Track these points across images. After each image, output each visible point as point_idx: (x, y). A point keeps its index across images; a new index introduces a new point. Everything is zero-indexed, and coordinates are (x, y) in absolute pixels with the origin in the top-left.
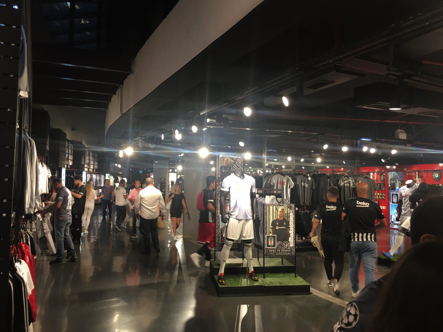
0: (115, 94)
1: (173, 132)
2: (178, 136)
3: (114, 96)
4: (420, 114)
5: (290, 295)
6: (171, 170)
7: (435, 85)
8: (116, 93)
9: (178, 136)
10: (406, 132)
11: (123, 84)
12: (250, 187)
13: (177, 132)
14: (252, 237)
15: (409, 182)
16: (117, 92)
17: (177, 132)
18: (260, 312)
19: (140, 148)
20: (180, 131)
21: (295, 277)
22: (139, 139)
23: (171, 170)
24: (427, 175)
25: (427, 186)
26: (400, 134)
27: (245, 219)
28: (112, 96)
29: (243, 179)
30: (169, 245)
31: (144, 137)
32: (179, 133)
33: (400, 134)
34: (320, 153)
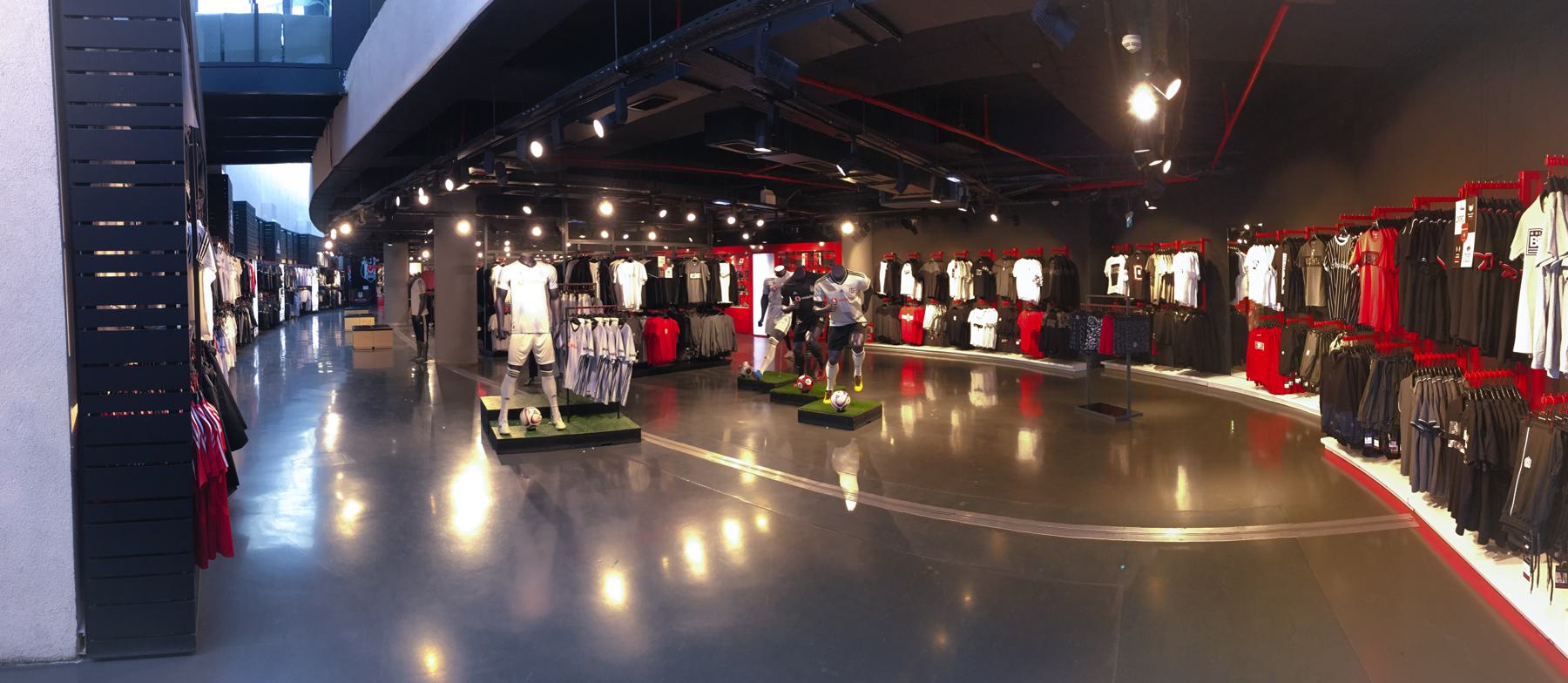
2: (423, 199)
9: (423, 199)
13: (421, 191)
20: (427, 192)
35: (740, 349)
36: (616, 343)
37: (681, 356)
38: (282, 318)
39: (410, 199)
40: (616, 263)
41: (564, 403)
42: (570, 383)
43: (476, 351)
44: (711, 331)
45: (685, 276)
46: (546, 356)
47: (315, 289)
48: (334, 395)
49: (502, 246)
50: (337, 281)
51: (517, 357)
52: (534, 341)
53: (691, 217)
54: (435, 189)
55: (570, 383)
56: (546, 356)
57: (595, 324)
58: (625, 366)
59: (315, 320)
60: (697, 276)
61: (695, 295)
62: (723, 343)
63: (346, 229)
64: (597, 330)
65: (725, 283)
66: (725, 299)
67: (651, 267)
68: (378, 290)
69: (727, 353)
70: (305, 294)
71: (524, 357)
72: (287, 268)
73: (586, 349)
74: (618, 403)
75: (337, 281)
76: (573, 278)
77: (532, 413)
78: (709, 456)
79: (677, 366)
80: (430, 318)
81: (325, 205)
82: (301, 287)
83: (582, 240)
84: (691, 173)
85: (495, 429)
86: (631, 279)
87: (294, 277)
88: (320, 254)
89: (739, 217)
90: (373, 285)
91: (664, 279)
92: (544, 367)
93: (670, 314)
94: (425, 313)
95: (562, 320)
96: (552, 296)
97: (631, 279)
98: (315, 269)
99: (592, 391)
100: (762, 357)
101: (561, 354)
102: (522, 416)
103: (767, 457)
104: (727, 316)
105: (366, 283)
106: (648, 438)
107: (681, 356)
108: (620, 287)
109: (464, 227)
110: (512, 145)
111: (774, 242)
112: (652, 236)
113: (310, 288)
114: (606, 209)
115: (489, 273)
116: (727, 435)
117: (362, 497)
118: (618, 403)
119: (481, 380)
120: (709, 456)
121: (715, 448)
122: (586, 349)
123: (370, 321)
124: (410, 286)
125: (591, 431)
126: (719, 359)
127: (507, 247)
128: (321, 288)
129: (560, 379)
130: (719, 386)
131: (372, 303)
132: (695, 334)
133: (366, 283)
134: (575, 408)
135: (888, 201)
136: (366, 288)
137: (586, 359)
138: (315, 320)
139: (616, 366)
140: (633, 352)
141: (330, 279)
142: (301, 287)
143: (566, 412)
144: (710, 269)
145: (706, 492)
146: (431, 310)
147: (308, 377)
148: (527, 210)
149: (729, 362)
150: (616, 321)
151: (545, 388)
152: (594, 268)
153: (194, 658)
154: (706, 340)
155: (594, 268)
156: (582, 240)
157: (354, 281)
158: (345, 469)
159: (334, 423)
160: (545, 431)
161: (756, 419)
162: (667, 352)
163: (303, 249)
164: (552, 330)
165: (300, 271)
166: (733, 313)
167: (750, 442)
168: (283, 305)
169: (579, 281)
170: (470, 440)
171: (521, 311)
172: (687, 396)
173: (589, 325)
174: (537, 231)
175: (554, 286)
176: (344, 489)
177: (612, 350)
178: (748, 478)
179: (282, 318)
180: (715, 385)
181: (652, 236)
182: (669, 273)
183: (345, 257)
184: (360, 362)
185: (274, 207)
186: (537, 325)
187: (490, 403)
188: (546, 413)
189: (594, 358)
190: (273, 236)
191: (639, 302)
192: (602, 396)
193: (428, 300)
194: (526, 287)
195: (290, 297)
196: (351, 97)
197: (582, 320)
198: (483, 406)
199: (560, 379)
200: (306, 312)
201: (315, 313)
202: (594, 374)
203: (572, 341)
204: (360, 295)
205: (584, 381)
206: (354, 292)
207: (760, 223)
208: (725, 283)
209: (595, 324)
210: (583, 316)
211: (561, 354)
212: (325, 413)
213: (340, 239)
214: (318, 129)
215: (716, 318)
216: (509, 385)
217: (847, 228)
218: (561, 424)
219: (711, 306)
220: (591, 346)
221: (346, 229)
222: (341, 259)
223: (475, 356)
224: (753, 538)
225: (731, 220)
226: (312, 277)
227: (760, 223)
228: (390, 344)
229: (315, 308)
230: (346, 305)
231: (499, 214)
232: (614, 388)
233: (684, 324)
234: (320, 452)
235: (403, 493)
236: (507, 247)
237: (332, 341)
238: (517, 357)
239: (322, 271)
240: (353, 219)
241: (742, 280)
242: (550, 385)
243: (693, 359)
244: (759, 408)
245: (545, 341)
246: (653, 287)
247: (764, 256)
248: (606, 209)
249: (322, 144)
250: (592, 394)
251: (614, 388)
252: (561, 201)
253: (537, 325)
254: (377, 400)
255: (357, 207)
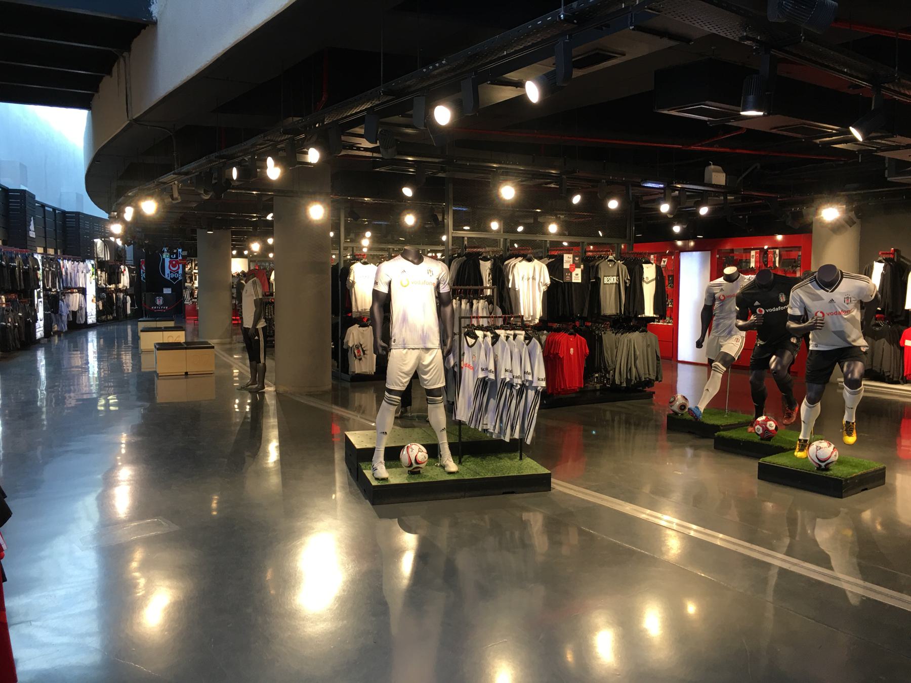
0: (109, 73)
1: (259, 163)
2: (273, 171)
3: (106, 80)
4: (774, 131)
5: (513, 493)
6: (234, 252)
7: (827, 67)
9: (273, 171)
10: (725, 171)
11: (129, 50)
12: (435, 282)
13: (270, 161)
15: (729, 270)
16: (115, 69)
17: (270, 161)
18: (896, 403)
19: (177, 199)
20: (278, 161)
21: (521, 459)
23: (234, 252)
26: (714, 174)
27: (421, 346)
28: (100, 79)
29: (418, 263)
30: (248, 407)
31: (186, 174)
32: (276, 165)
33: (714, 174)
34: (556, 215)
35: (665, 380)
36: (520, 362)
37: (598, 386)
38: (40, 332)
39: (252, 173)
40: (512, 261)
41: (455, 440)
42: (463, 413)
44: (627, 351)
45: (598, 280)
46: (435, 379)
47: (91, 292)
48: (124, 438)
49: (360, 235)
50: (125, 281)
51: (397, 379)
52: (419, 359)
53: (613, 204)
54: (290, 157)
55: (463, 413)
56: (435, 379)
57: (496, 338)
58: (531, 394)
59: (92, 337)
60: (613, 280)
61: (610, 305)
62: (643, 369)
63: (150, 207)
64: (499, 344)
65: (649, 291)
66: (649, 311)
67: (555, 268)
68: (186, 294)
69: (649, 383)
70: (75, 300)
71: (406, 380)
72: (47, 259)
73: (485, 369)
74: (522, 440)
75: (125, 281)
76: (465, 282)
77: (416, 451)
78: (628, 508)
79: (581, 397)
80: (269, 333)
81: (114, 169)
82: (69, 289)
84: (625, 152)
85: (368, 473)
86: (529, 281)
87: (57, 274)
88: (99, 242)
89: (676, 203)
90: (179, 286)
91: (571, 284)
92: (430, 392)
93: (577, 331)
94: (262, 324)
95: (453, 333)
96: (442, 301)
97: (529, 281)
98: (90, 264)
99: (490, 424)
100: (693, 389)
101: (453, 376)
102: (404, 454)
103: (697, 508)
105: (168, 284)
106: (558, 485)
107: (598, 386)
108: (516, 293)
109: (317, 212)
110: (404, 109)
111: (712, 238)
112: (553, 228)
113: (83, 291)
114: (508, 192)
115: (347, 272)
116: (647, 489)
117: (179, 572)
118: (522, 440)
119: (338, 410)
120: (628, 508)
121: (631, 500)
122: (485, 369)
123: (179, 337)
124: (240, 288)
125: (490, 475)
126: (639, 389)
128: (99, 290)
129: (451, 408)
130: (637, 425)
131: (177, 311)
132: (607, 355)
133: (168, 284)
134: (468, 445)
135: (631, 380)
136: (167, 291)
137: (484, 382)
138: (92, 337)
139: (520, 393)
140: (543, 375)
141: (114, 277)
142: (69, 289)
143: (458, 451)
144: (631, 271)
145: (622, 558)
146: (270, 322)
148: (408, 192)
149: (651, 395)
150: (521, 334)
152: (486, 267)
154: (621, 360)
155: (486, 267)
156: (466, 232)
157: (150, 283)
158: (148, 542)
160: (433, 475)
161: (686, 469)
162: (573, 379)
163: (72, 235)
164: (443, 343)
165: (67, 265)
166: (656, 330)
168: (40, 315)
169: (472, 284)
170: (329, 489)
171: (404, 319)
172: (592, 446)
173: (489, 340)
174: (410, 220)
175: (445, 289)
176: (146, 566)
177: (517, 372)
178: (673, 546)
179: (40, 332)
181: (553, 228)
182: (577, 277)
184: (165, 393)
185: (23, 167)
187: (358, 439)
188: (433, 451)
189: (494, 382)
191: (539, 312)
192: (502, 431)
193: (265, 306)
194: (411, 287)
195: (52, 304)
196: (162, 29)
197: (479, 333)
199: (451, 408)
200: (77, 326)
201: (92, 326)
202: (493, 402)
203: (466, 359)
204: (159, 301)
205: (481, 410)
206: (150, 293)
207: (704, 211)
208: (649, 291)
209: (496, 338)
210: (481, 328)
211: (453, 376)
212: (114, 468)
213: (140, 224)
215: (636, 336)
216: (388, 413)
217: (215, 513)
218: (452, 466)
219: (630, 319)
220: (491, 367)
221: (150, 207)
222: (129, 250)
223: (328, 383)
224: (676, 621)
226: (86, 276)
227: (704, 211)
228: (212, 368)
229: (92, 319)
230: (138, 314)
231: (365, 194)
232: (518, 421)
233: (595, 343)
234: (107, 522)
235: (232, 572)
238: (397, 379)
239: (101, 265)
240: (161, 192)
241: (668, 286)
242: (438, 415)
243: (603, 389)
245: (434, 358)
246: (557, 294)
247: (696, 254)
248: (508, 192)
249: (109, 85)
250: (490, 428)
251: (518, 421)
252: (452, 182)
253: (424, 338)
254: (188, 446)
255: (170, 177)
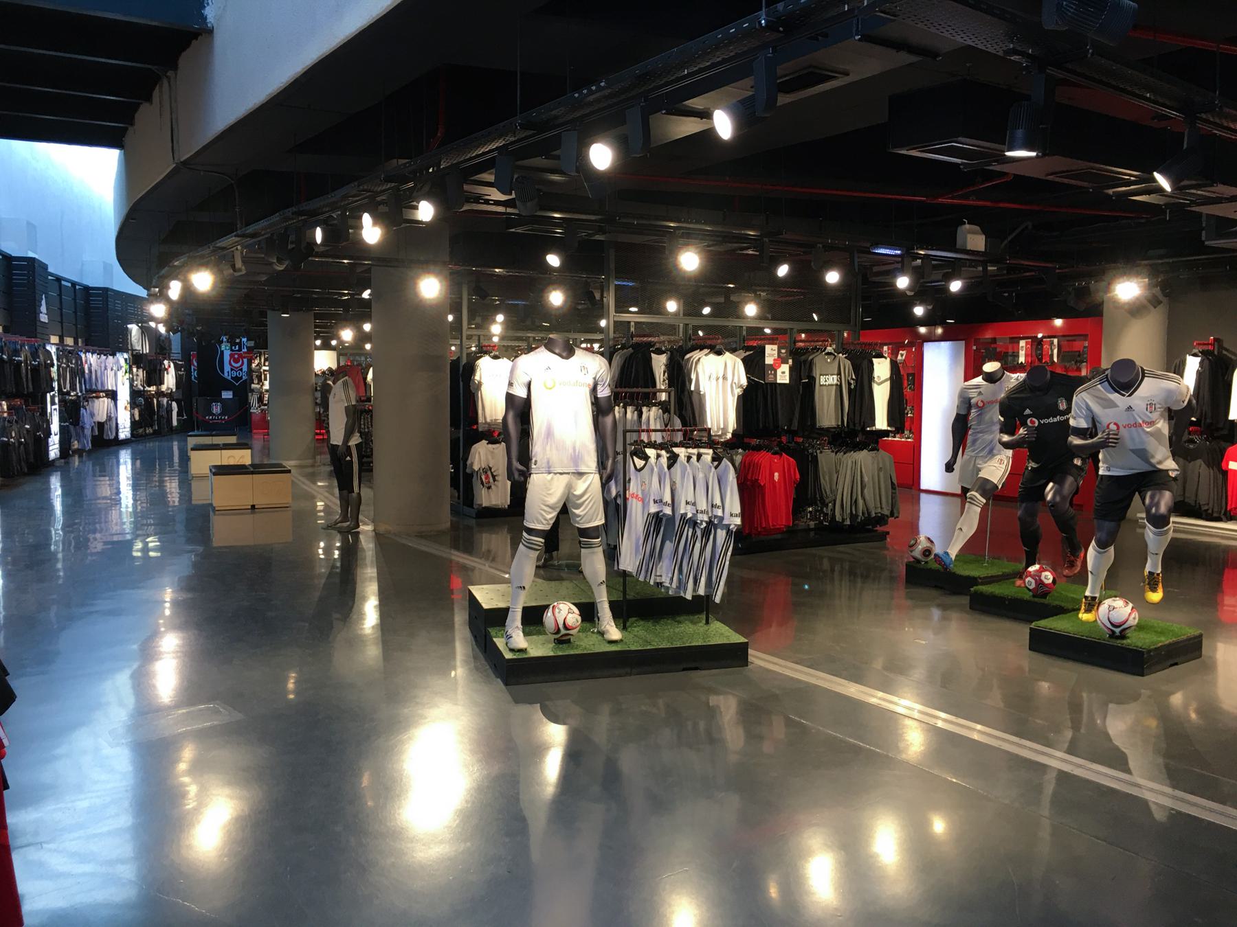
0: (149, 99)
1: (351, 222)
2: (371, 232)
3: (145, 108)
4: (1050, 178)
5: (696, 669)
6: (318, 342)
7: (1123, 90)
8: (151, 96)
9: (371, 232)
11: (175, 67)
12: (591, 382)
13: (367, 219)
14: (599, 521)
16: (156, 93)
17: (367, 219)
18: (1216, 547)
19: (240, 270)
20: (377, 219)
21: (707, 623)
22: (234, 244)
23: (318, 342)
24: (649, 437)
25: (1049, 375)
26: (969, 236)
28: (136, 107)
29: (567, 357)
30: (337, 552)
31: (253, 236)
32: (375, 224)
33: (969, 236)
34: (755, 292)
35: (903, 515)
36: (707, 491)
37: (811, 524)
38: (54, 451)
39: (342, 235)
40: (696, 355)
41: (618, 596)
42: (629, 561)
43: (447, 508)
44: (852, 476)
45: (812, 380)
46: (591, 514)
47: (124, 396)
48: (168, 595)
50: (170, 381)
51: (540, 514)
52: (569, 487)
53: (833, 277)
55: (629, 561)
56: (591, 514)
57: (673, 459)
58: (721, 534)
59: (125, 457)
60: (833, 380)
61: (828, 414)
62: (874, 500)
63: (203, 281)
64: (677, 466)
65: (881, 394)
66: (881, 423)
67: (754, 364)
68: (253, 399)
69: (881, 520)
70: (101, 407)
71: (552, 516)
72: (64, 352)
73: (659, 501)
74: (708, 598)
75: (170, 381)
76: (631, 383)
77: (565, 613)
78: (853, 690)
79: (790, 539)
80: (365, 452)
81: (154, 230)
82: (93, 392)
83: (633, 315)
84: (849, 206)
85: (500, 642)
86: (719, 382)
87: (78, 372)
88: (134, 328)
90: (242, 389)
91: (775, 385)
92: (584, 533)
93: (784, 449)
94: (355, 440)
95: (615, 452)
96: (600, 409)
97: (719, 382)
98: (122, 358)
99: (665, 575)
100: (941, 529)
101: (616, 510)
102: (548, 616)
103: (946, 689)
104: (882, 453)
105: (227, 385)
106: (757, 658)
107: (811, 524)
109: (430, 288)
111: (967, 323)
112: (751, 310)
113: (113, 395)
114: (690, 261)
115: (470, 369)
116: (878, 664)
117: (244, 777)
118: (708, 598)
119: (459, 557)
120: (853, 690)
121: (857, 678)
122: (659, 501)
123: (243, 457)
124: (326, 391)
125: (665, 645)
126: (867, 528)
127: (497, 328)
128: (135, 394)
129: (612, 554)
130: (865, 577)
131: (240, 423)
132: (825, 482)
133: (227, 385)
134: (636, 604)
136: (227, 395)
137: (657, 519)
138: (125, 457)
139: (706, 533)
140: (737, 509)
141: (155, 376)
142: (93, 392)
143: (622, 612)
144: (856, 368)
145: (845, 757)
146: (367, 437)
147: (112, 571)
148: (553, 260)
149: (884, 536)
151: (586, 568)
152: (659, 363)
153: (504, 687)
155: (659, 363)
156: (633, 315)
157: (203, 384)
158: (201, 736)
159: (171, 643)
160: (588, 644)
161: (930, 636)
162: (778, 514)
163: (97, 318)
164: (601, 465)
165: (91, 360)
166: (890, 448)
167: (919, 673)
168: (55, 427)
169: (641, 385)
171: (549, 434)
172: (804, 605)
173: (664, 461)
174: (556, 298)
175: (604, 392)
176: (198, 768)
177: (702, 505)
178: (914, 741)
179: (54, 451)
180: (864, 574)
181: (751, 310)
182: (783, 375)
183: (187, 335)
184: (224, 533)
185: (31, 226)
186: (576, 459)
187: (487, 596)
188: (588, 612)
189: (671, 519)
190: (31, 285)
191: (732, 424)
192: (682, 585)
193: (360, 415)
194: (558, 389)
195: (71, 412)
196: (219, 39)
197: (651, 452)
198: (473, 601)
199: (612, 554)
200: (105, 443)
201: (125, 443)
202: (669, 546)
203: (633, 488)
204: (217, 409)
205: (654, 556)
206: (204, 398)
207: (956, 286)
208: (881, 394)
209: (673, 459)
210: (653, 445)
211: (616, 510)
212: (154, 635)
213: (190, 304)
214: (142, 88)
215: (863, 457)
216: (526, 561)
218: (614, 633)
219: (855, 433)
220: (667, 498)
221: (203, 281)
222: (176, 339)
223: (445, 519)
224: (918, 844)
225: (903, 282)
226: (117, 375)
227: (956, 286)
228: (288, 500)
229: (124, 433)
230: (188, 427)
231: (495, 263)
232: (703, 572)
233: (807, 465)
234: (146, 709)
235: (315, 776)
236: (497, 328)
237: (159, 499)
238: (540, 514)
239: (137, 360)
240: (218, 260)
241: (907, 388)
242: (594, 563)
243: (819, 528)
244: (928, 618)
245: (589, 486)
246: (756, 399)
247: (945, 345)
248: (690, 261)
249: (147, 115)
250: (666, 580)
251: (703, 572)
252: (613, 247)
253: (576, 459)
254: (255, 606)
